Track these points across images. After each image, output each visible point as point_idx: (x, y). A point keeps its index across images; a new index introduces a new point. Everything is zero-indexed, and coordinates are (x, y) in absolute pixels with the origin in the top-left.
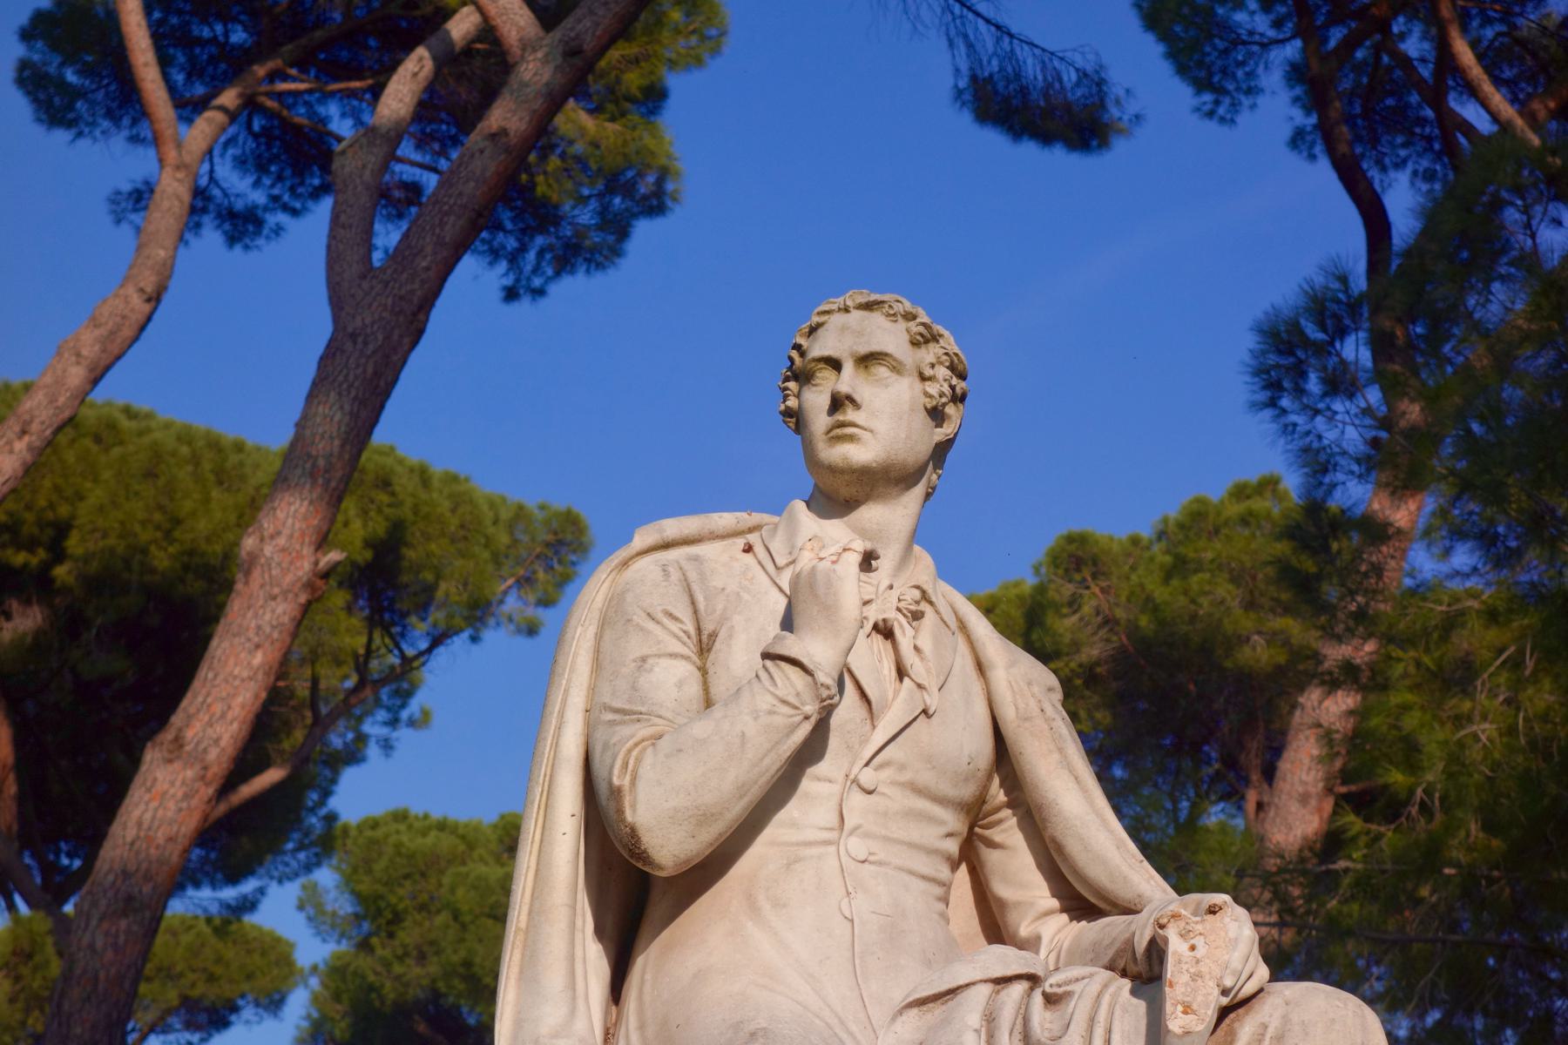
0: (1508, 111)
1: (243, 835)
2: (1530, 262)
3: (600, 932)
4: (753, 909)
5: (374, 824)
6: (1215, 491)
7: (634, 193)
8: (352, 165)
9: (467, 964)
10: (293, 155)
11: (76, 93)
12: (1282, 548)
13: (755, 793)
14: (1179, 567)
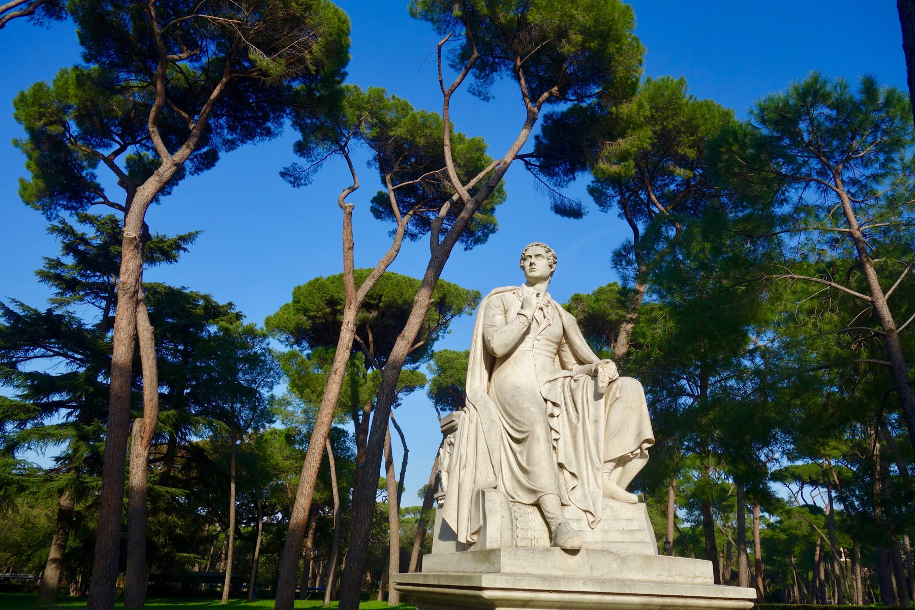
0: (662, 209)
1: (416, 354)
2: (667, 238)
3: (486, 368)
4: (516, 363)
6: (604, 285)
7: (489, 229)
8: (435, 225)
10: (423, 223)
11: (382, 212)
12: (618, 296)
13: (516, 341)
14: (597, 300)
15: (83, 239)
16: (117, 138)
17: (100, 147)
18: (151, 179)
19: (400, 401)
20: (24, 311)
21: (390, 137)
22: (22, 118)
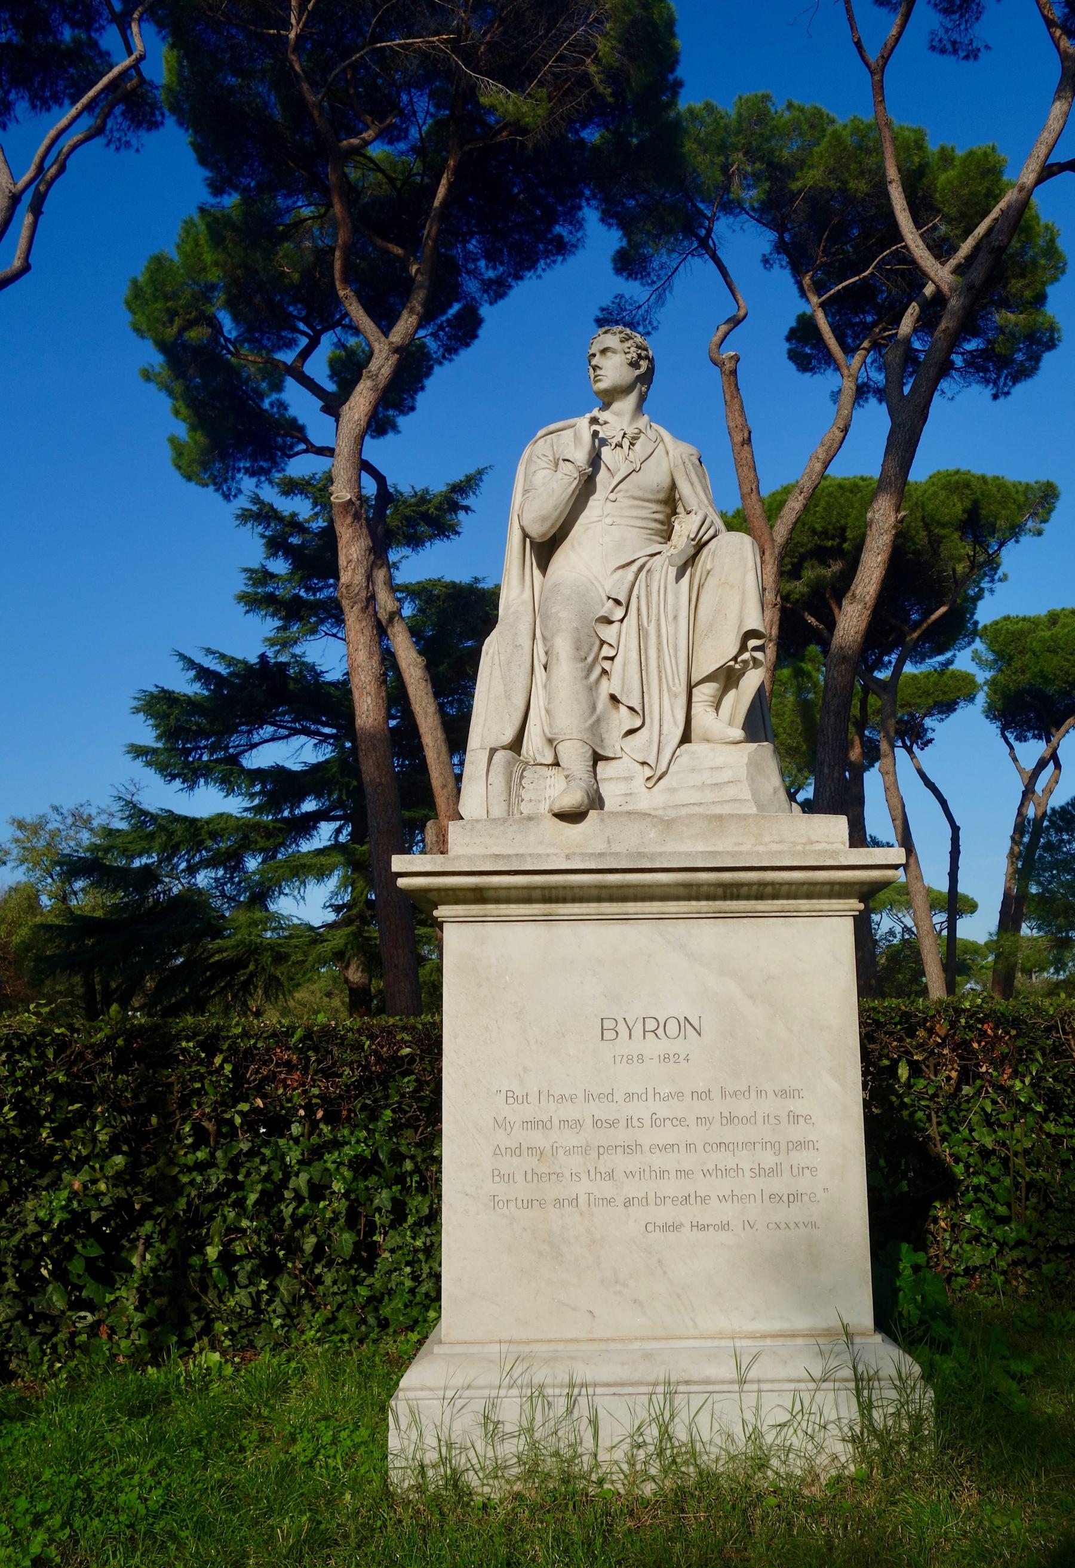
5: (997, 623)
9: (1041, 671)
15: (295, 525)
16: (302, 326)
17: (280, 349)
18: (360, 387)
19: (930, 735)
20: (229, 666)
21: (795, 195)
22: (144, 327)
